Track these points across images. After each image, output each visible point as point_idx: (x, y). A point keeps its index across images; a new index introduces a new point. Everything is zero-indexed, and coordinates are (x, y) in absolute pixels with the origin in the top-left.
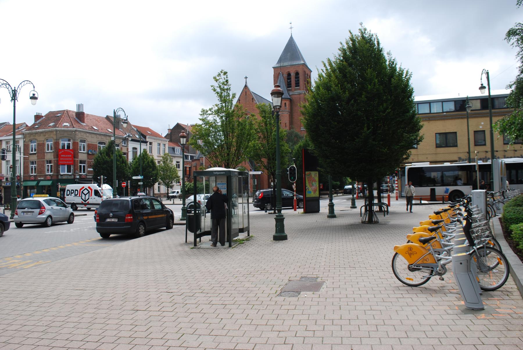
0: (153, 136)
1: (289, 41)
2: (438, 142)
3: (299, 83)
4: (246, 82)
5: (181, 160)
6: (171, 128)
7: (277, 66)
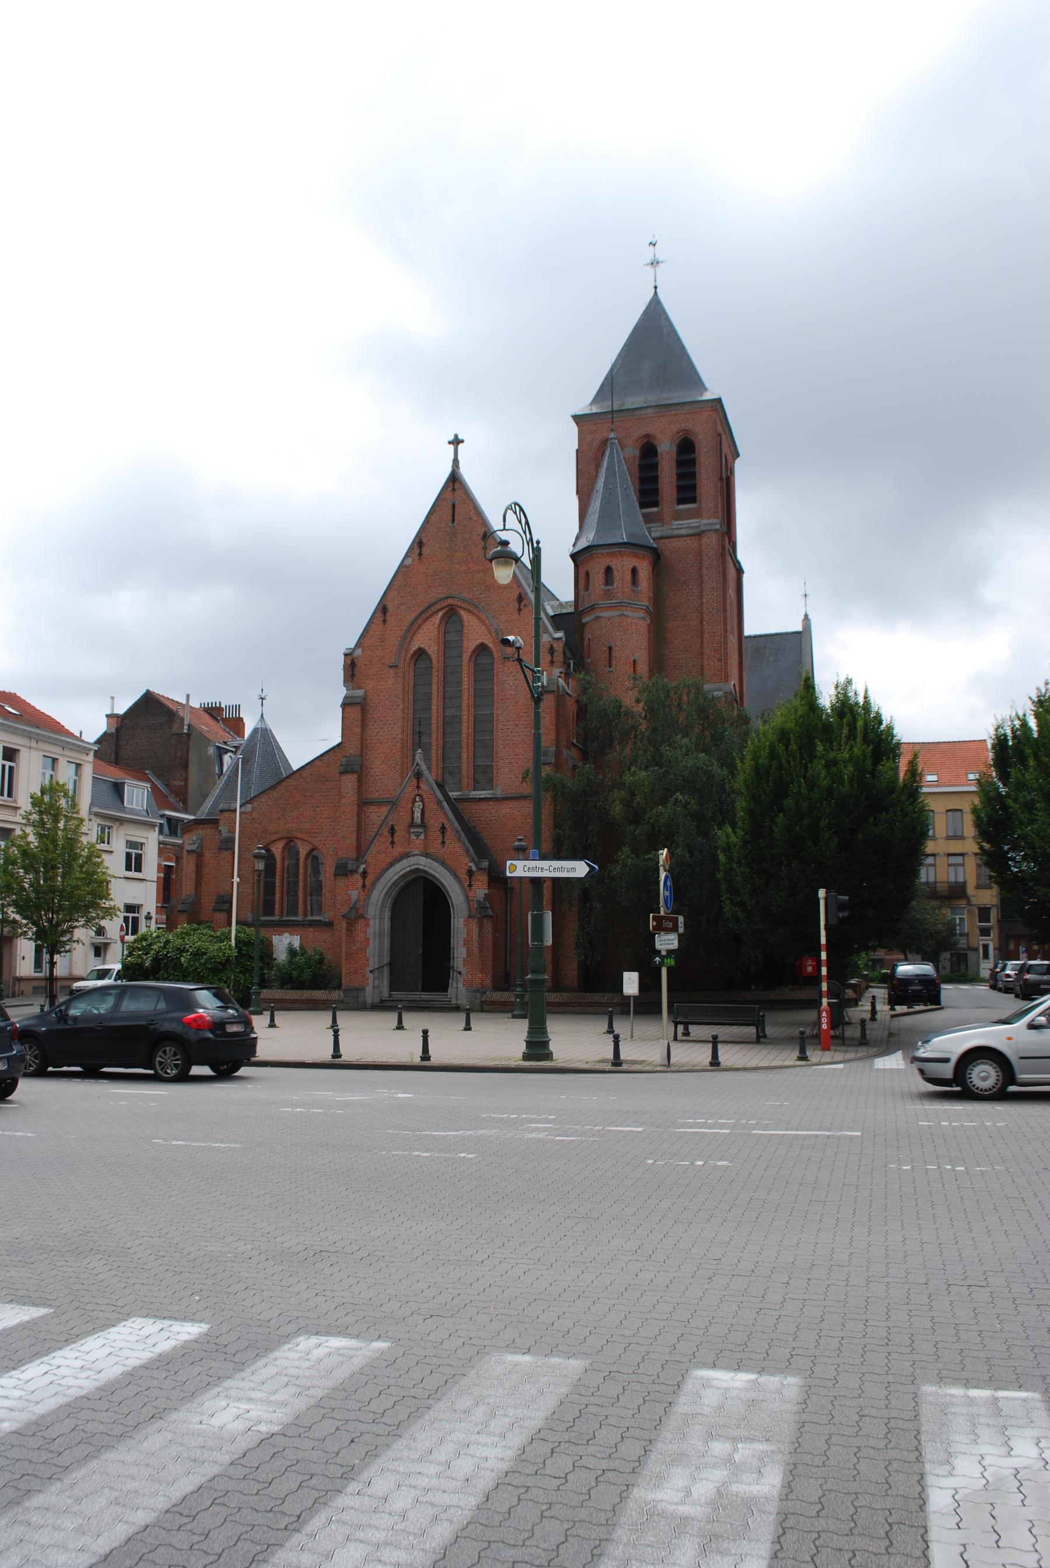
0: (30, 723)
1: (646, 313)
3: (693, 487)
4: (456, 461)
5: (151, 841)
6: (121, 709)
7: (595, 410)
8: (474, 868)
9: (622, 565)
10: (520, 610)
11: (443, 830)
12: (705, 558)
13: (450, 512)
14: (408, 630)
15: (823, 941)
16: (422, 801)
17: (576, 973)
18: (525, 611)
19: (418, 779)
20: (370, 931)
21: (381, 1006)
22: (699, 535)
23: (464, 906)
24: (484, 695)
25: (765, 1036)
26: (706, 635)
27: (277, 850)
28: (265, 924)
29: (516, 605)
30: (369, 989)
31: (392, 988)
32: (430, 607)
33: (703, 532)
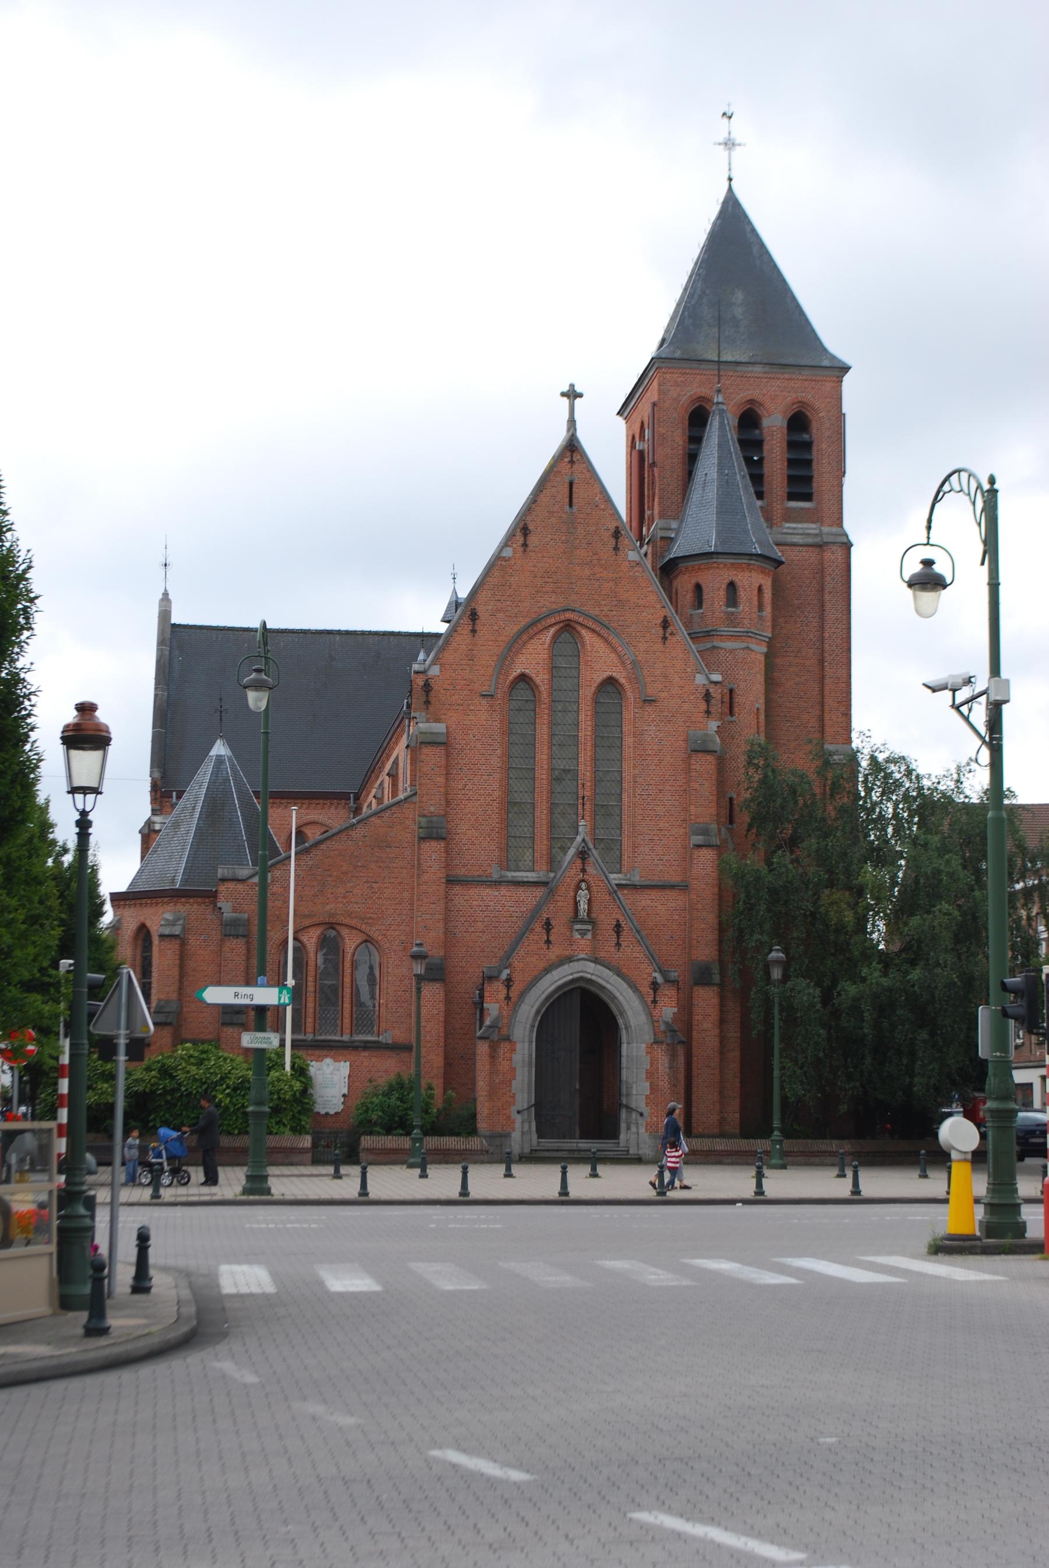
1: (725, 203)
3: (808, 480)
4: (572, 422)
8: (660, 979)
10: (665, 638)
12: (828, 578)
13: (567, 490)
16: (588, 888)
17: (737, 1116)
18: (672, 640)
19: (583, 859)
22: (820, 546)
24: (608, 740)
26: (827, 681)
29: (661, 631)
30: (516, 1135)
31: (541, 1135)
33: (827, 543)
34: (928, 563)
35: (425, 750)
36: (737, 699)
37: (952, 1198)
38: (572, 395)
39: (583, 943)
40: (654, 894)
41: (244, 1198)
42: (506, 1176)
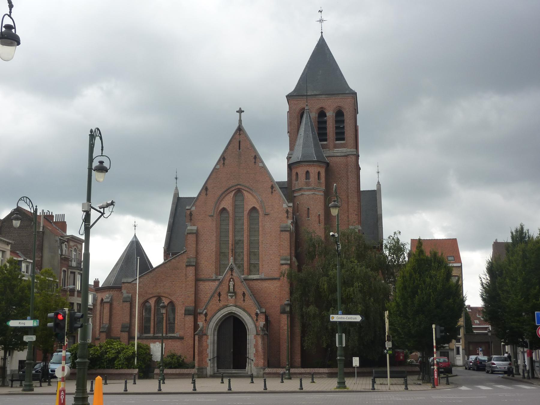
2: (18, 385)
3: (343, 133)
4: (240, 121)
8: (259, 312)
9: (313, 170)
10: (272, 192)
11: (244, 294)
13: (238, 144)
14: (218, 200)
15: (434, 344)
16: (234, 281)
17: (300, 360)
20: (209, 341)
21: (214, 376)
23: (255, 329)
24: (254, 230)
25: (374, 389)
26: (350, 203)
27: (152, 302)
28: (147, 338)
30: (209, 369)
32: (228, 189)
33: (348, 155)
34: (101, 162)
35: (189, 236)
36: (311, 212)
37: (95, 392)
38: (240, 111)
39: (232, 301)
40: (269, 282)
41: (338, 390)
42: (251, 383)
